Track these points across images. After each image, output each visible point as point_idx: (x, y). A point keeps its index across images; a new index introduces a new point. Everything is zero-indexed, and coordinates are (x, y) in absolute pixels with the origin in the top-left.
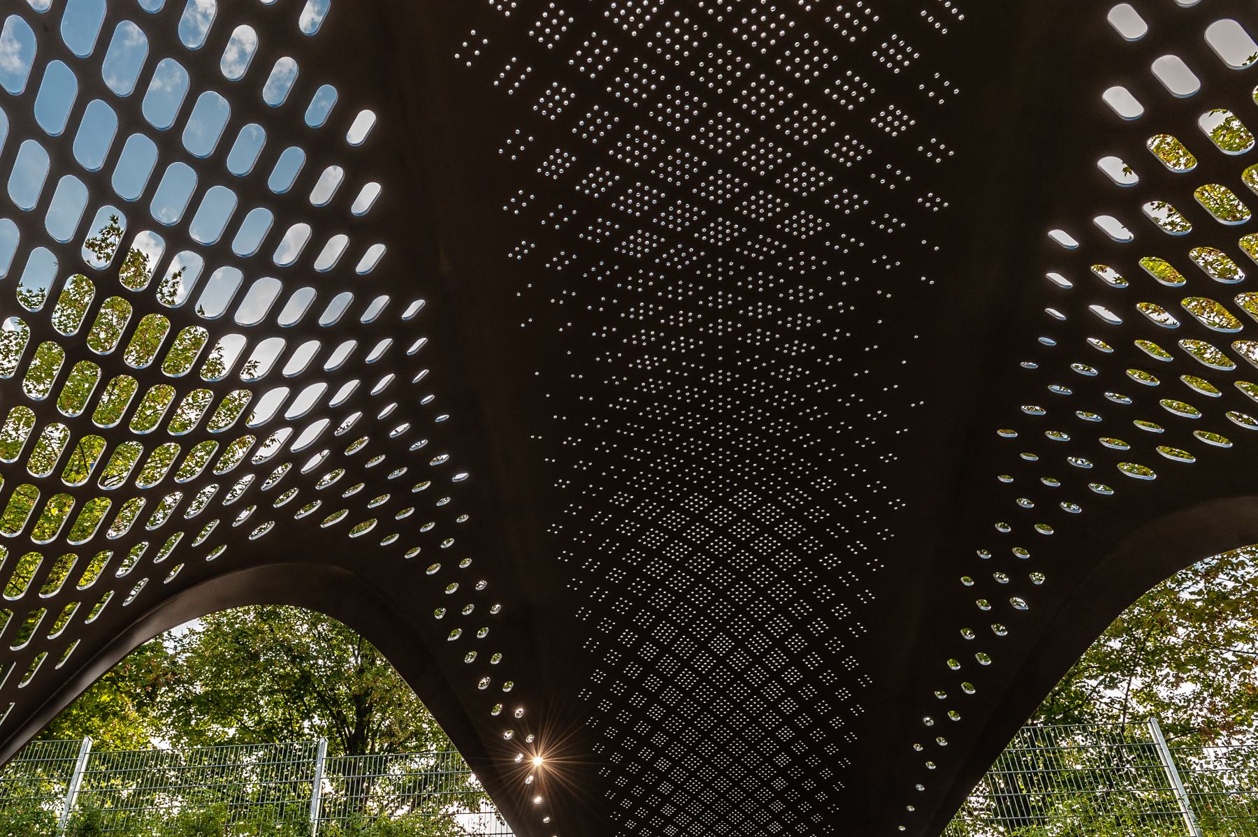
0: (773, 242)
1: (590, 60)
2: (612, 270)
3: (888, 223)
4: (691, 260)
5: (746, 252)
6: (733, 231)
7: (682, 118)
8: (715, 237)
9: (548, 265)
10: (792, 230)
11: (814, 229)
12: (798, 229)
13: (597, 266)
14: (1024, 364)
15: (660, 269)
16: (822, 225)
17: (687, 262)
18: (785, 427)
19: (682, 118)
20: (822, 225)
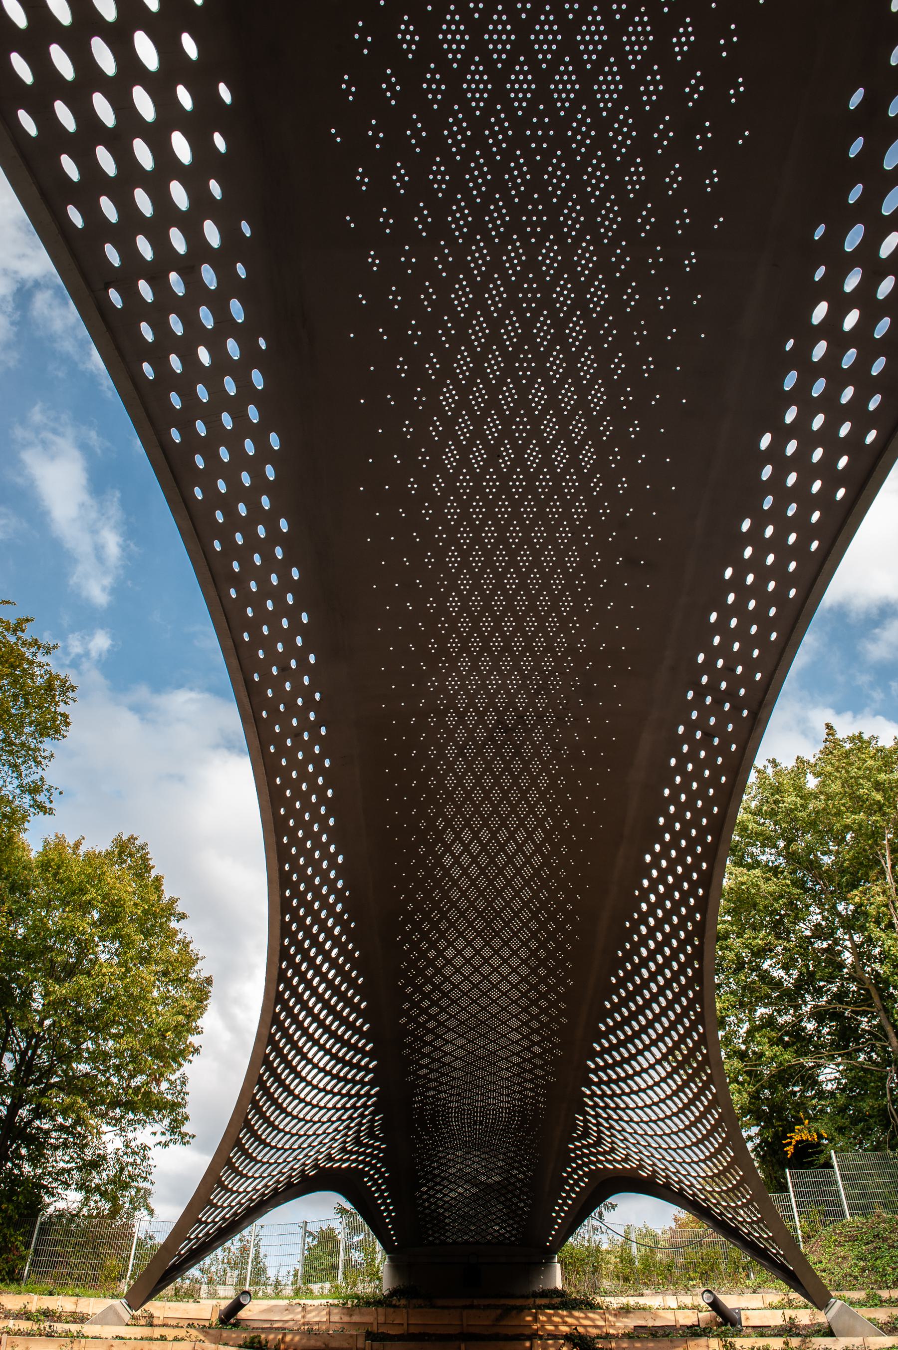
0: (509, 268)
1: (559, 173)
2: (496, 154)
3: (694, 89)
4: (466, 286)
5: (693, 82)
6: (453, 21)
7: (482, 95)
8: (449, 31)
9: (680, 232)
10: (549, 50)
11: (586, 51)
12: (550, 44)
13: (467, 129)
14: (788, 348)
15: (526, 198)
16: (453, 552)
17: (466, 212)
18: (407, 31)
19: (482, 95)
20: (453, 552)
